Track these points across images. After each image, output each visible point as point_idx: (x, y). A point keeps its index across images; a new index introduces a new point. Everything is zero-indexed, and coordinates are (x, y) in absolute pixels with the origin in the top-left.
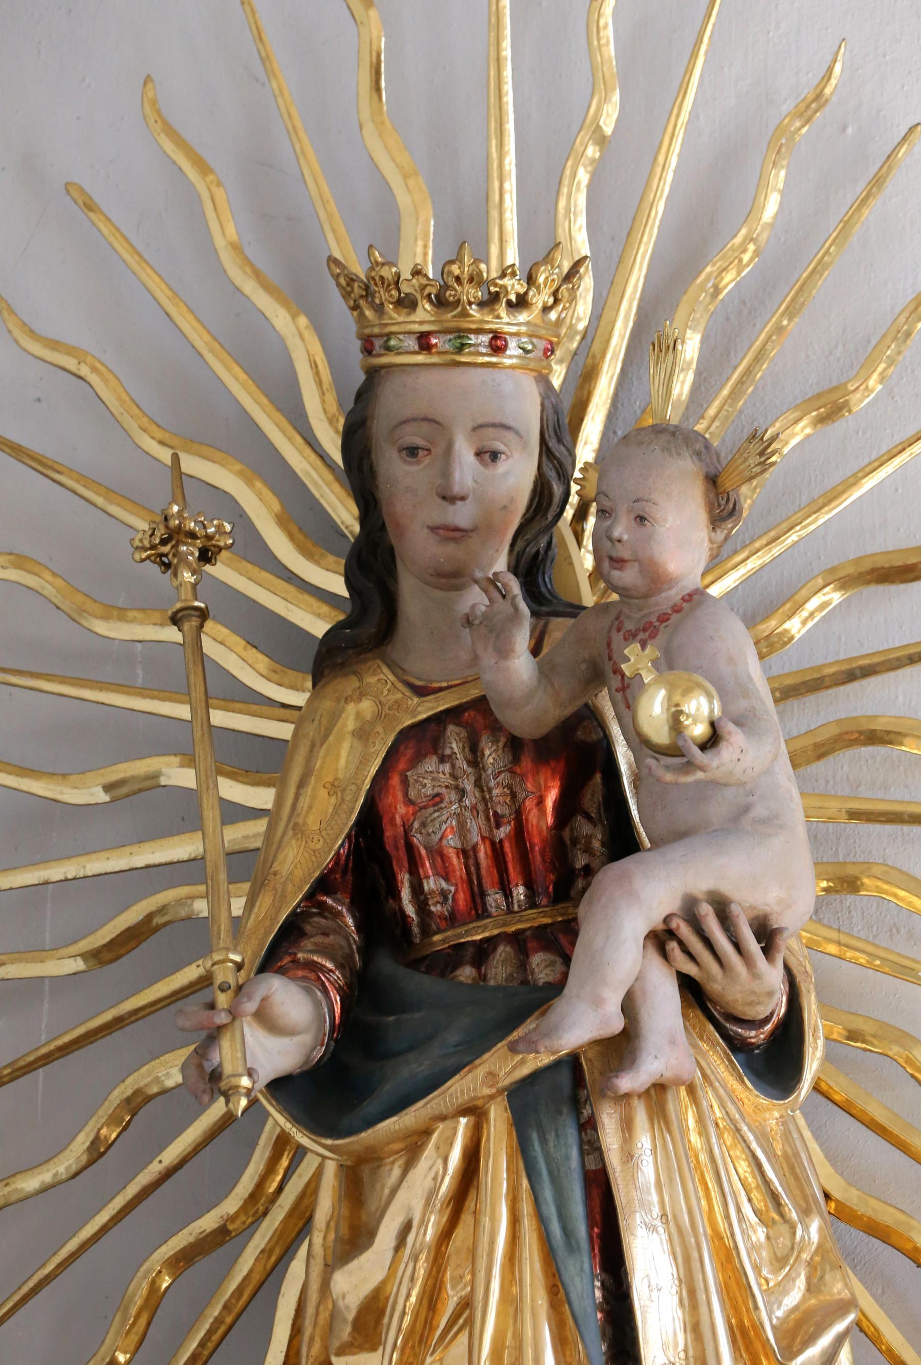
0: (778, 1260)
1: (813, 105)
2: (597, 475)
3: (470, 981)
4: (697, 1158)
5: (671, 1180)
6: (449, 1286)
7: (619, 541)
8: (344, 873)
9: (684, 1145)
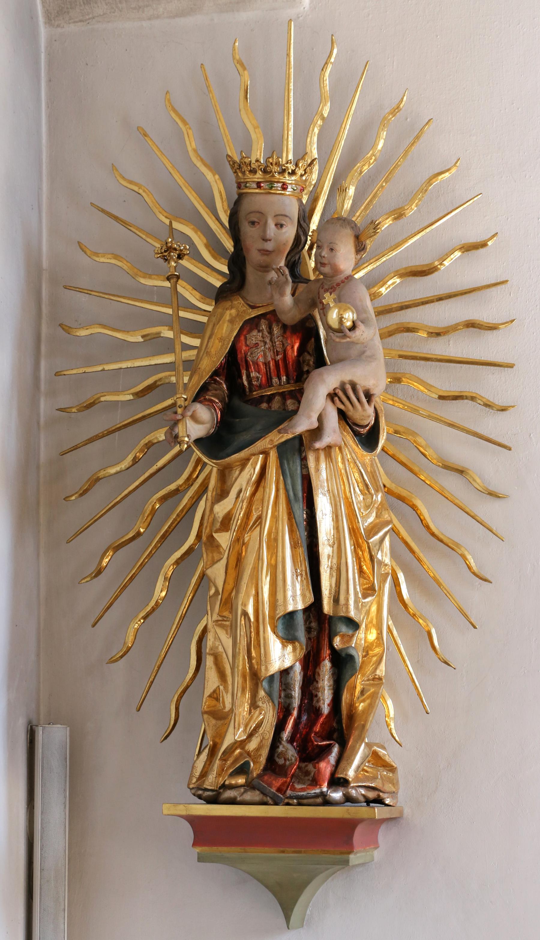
0: (367, 506)
1: (396, 110)
2: (317, 234)
3: (265, 408)
4: (341, 471)
5: (332, 478)
6: (254, 511)
7: (324, 257)
8: (223, 369)
9: (337, 467)
